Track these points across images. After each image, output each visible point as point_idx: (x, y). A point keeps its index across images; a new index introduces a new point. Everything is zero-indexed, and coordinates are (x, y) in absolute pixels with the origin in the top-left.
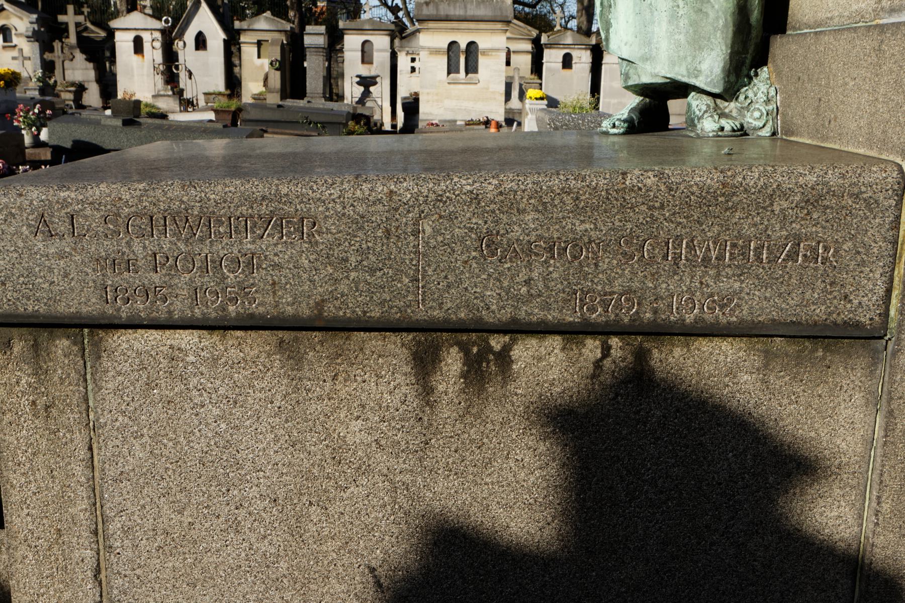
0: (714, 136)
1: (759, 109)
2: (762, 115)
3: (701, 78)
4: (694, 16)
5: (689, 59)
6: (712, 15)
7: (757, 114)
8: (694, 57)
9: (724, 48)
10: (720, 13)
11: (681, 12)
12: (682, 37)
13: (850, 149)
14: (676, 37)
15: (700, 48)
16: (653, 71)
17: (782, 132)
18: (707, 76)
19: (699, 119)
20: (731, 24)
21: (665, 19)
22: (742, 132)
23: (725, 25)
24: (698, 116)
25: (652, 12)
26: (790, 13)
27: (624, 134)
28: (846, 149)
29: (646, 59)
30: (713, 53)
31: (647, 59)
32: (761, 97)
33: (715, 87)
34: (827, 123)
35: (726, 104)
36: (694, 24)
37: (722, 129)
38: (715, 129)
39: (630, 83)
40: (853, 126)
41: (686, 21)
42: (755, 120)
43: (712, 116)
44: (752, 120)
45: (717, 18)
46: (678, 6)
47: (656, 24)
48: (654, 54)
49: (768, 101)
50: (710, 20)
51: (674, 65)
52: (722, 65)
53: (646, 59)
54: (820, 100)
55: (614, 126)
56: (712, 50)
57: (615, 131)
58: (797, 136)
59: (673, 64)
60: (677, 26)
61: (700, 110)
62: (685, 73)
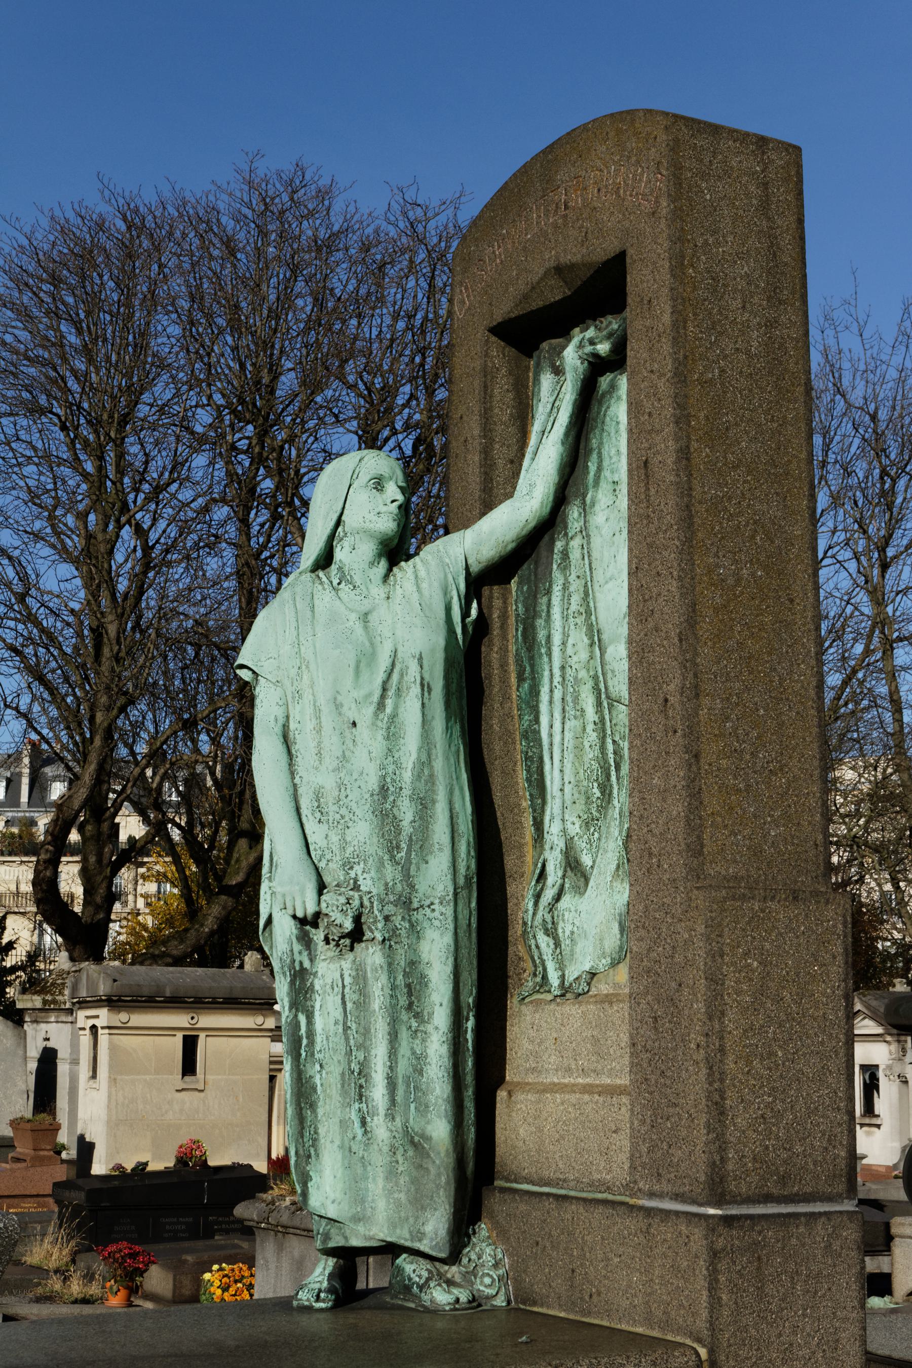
0: (451, 1310)
1: (488, 1275)
2: (493, 1280)
3: (425, 1242)
4: (415, 1173)
5: (411, 1220)
6: (433, 1171)
7: (487, 1280)
8: (417, 1218)
9: (447, 1207)
10: (442, 1169)
11: (401, 1169)
12: (402, 1196)
13: (624, 1327)
14: (396, 1195)
15: (423, 1208)
16: (367, 1233)
17: (516, 1299)
18: (432, 1240)
19: (421, 1288)
20: (453, 1181)
21: (381, 1175)
22: (475, 1301)
23: (447, 1183)
24: (418, 1284)
25: (364, 1166)
26: (497, 1160)
27: (332, 1308)
28: (619, 1327)
29: (357, 1219)
30: (437, 1213)
31: (360, 1220)
32: (487, 1259)
33: (440, 1251)
34: (587, 1298)
35: (446, 1268)
36: (414, 1181)
37: (457, 1300)
38: (452, 1301)
39: (331, 1244)
40: (625, 1303)
41: (407, 1179)
42: (486, 1286)
43: (439, 1285)
44: (485, 1285)
45: (439, 1175)
46: (397, 1162)
47: (370, 1180)
48: (369, 1214)
49: (496, 1266)
50: (432, 1177)
51: (395, 1227)
52: (446, 1226)
53: (357, 1219)
54: (573, 1271)
55: (318, 1298)
56: (435, 1209)
57: (322, 1305)
58: (542, 1306)
59: (393, 1226)
60: (397, 1184)
61: (420, 1277)
62: (408, 1236)
